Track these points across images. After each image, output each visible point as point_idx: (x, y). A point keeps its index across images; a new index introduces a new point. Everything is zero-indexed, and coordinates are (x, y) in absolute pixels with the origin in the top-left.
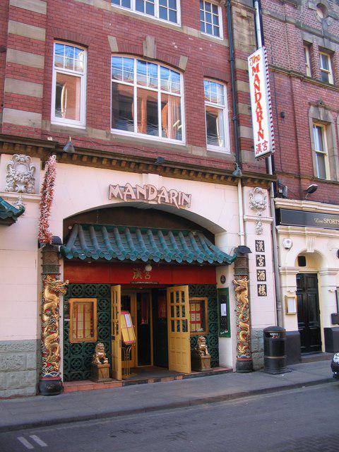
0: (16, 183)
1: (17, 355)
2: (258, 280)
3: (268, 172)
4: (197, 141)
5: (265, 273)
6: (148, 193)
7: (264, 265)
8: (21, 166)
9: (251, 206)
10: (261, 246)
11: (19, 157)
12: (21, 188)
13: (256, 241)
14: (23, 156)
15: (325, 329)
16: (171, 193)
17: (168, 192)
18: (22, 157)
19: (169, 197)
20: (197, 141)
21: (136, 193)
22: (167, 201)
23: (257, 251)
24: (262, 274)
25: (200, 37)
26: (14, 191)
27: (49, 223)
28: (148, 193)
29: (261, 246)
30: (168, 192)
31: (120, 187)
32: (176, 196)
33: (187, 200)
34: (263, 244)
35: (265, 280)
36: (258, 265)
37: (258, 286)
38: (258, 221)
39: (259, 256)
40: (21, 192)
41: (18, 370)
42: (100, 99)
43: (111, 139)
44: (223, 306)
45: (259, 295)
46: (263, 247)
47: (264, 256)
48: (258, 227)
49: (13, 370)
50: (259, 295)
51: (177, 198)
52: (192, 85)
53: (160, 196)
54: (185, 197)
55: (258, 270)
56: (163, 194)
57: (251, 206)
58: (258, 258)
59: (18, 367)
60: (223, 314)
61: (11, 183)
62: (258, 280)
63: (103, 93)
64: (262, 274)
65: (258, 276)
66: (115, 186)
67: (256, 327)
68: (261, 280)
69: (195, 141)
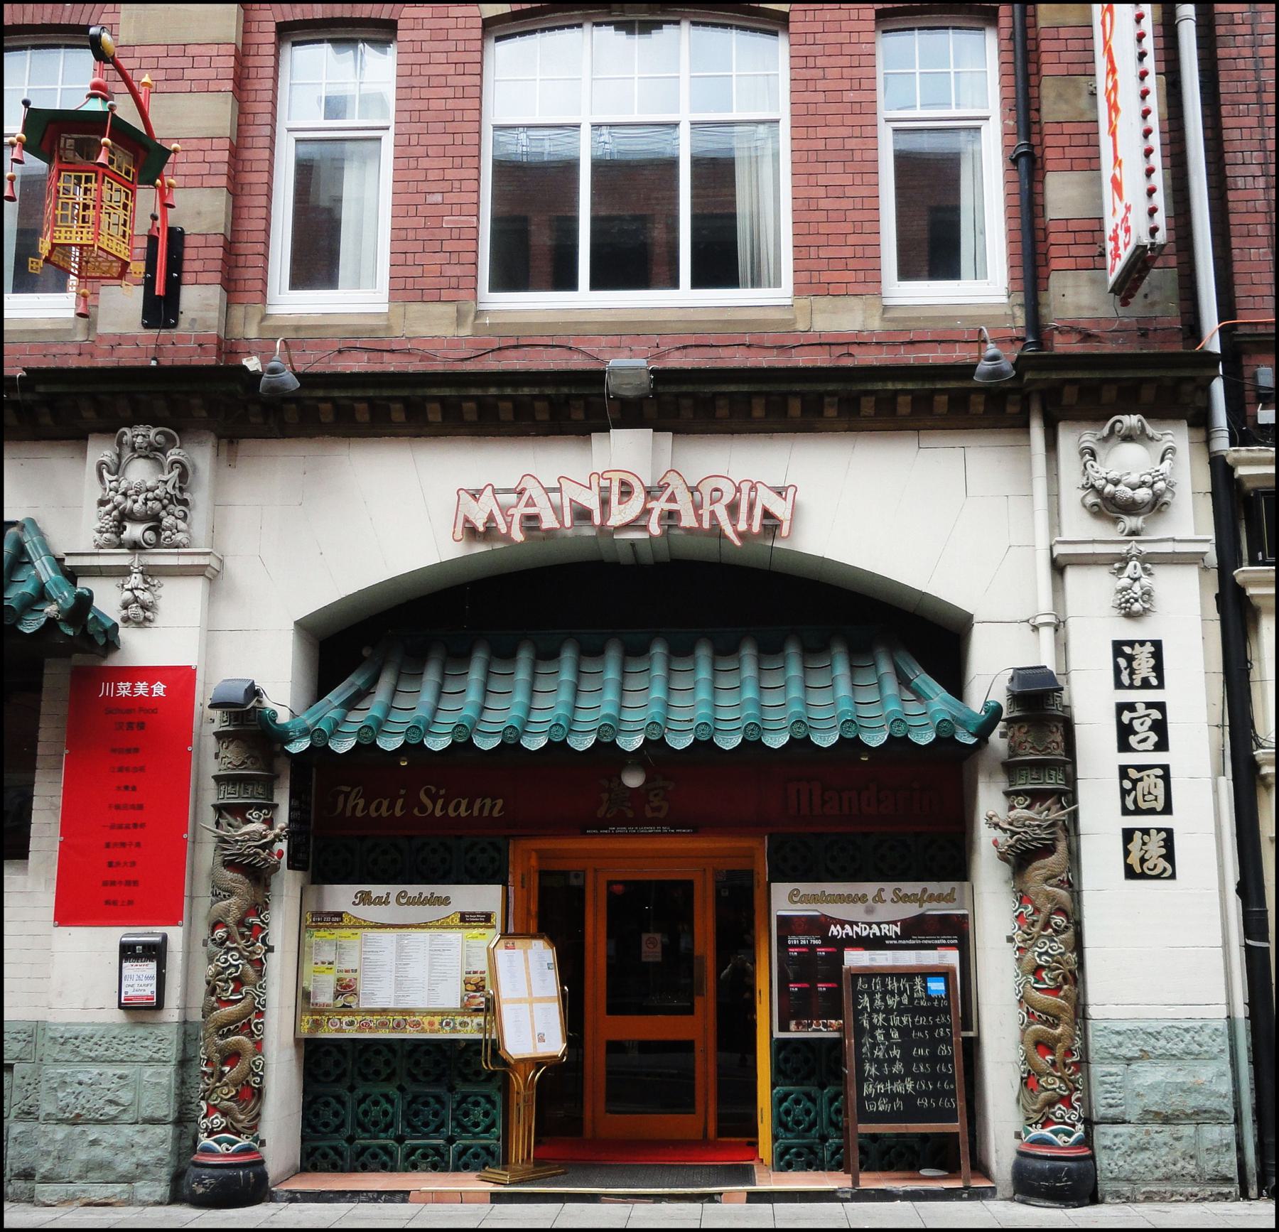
0: (124, 517)
1: (110, 1071)
2: (1126, 811)
3: (1193, 329)
4: (836, 276)
5: (1166, 778)
6: (605, 503)
7: (1162, 745)
8: (142, 461)
9: (1091, 499)
10: (1144, 666)
11: (128, 434)
12: (134, 531)
13: (1118, 647)
14: (141, 430)
15: (779, 917)
16: (706, 489)
17: (692, 490)
18: (138, 434)
19: (697, 507)
20: (836, 276)
21: (557, 510)
22: (688, 520)
23: (1119, 685)
24: (1151, 782)
25: (892, 326)
26: (121, 546)
27: (161, 604)
28: (605, 503)
29: (1144, 666)
30: (692, 490)
31: (495, 492)
32: (727, 499)
33: (781, 509)
34: (1157, 654)
35: (1167, 810)
36: (1124, 746)
37: (1128, 835)
38: (1124, 560)
39: (1131, 707)
40: (135, 546)
41: (113, 1120)
42: (438, 198)
43: (475, 327)
44: (1260, 554)
45: (1130, 873)
46: (1158, 669)
47: (1161, 707)
48: (1125, 582)
49: (99, 1122)
50: (1130, 873)
51: (733, 509)
52: (821, 62)
53: (659, 506)
54: (766, 499)
55: (1123, 771)
56: (672, 499)
57: (1091, 499)
58: (1126, 717)
59: (112, 1110)
60: (924, 1172)
61: (109, 522)
62: (1126, 811)
63: (450, 174)
64: (1151, 782)
65: (1124, 793)
66: (480, 492)
67: (1112, 1012)
68: (1138, 811)
69: (825, 277)
